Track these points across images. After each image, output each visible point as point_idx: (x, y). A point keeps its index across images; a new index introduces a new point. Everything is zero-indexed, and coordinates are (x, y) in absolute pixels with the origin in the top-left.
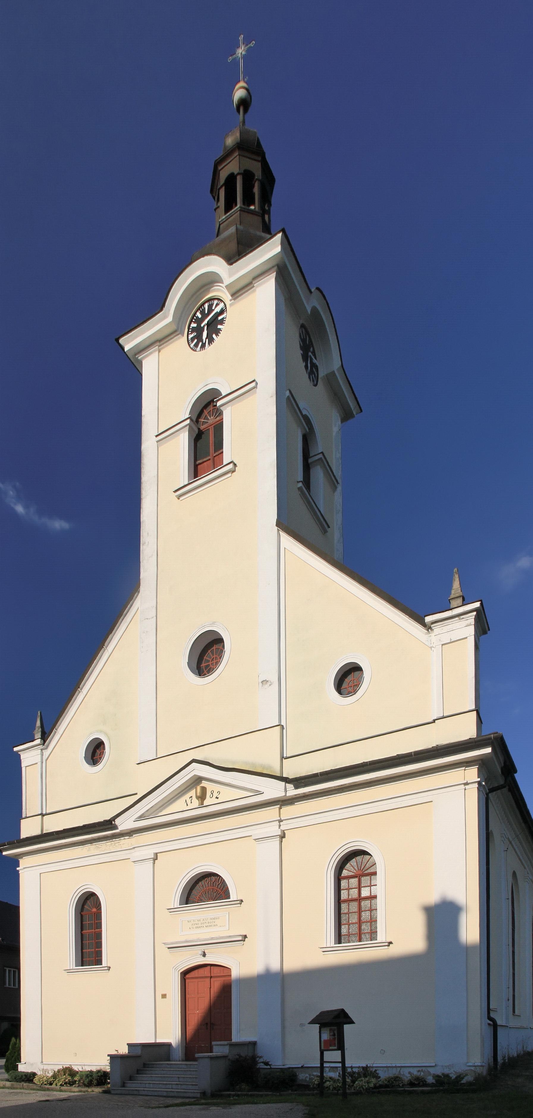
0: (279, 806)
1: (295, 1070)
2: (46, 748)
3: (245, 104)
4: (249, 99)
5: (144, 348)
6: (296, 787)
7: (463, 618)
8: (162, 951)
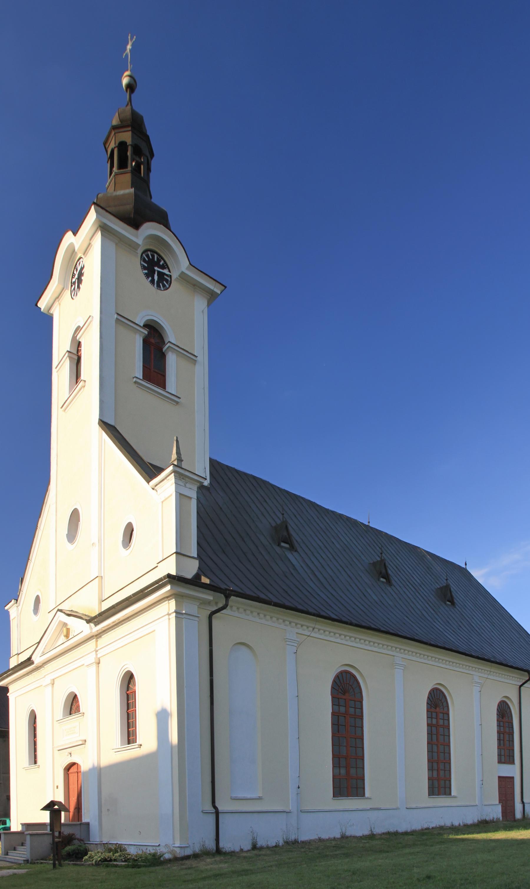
0: (94, 640)
3: (131, 87)
4: (133, 82)
6: (96, 625)
8: (56, 752)
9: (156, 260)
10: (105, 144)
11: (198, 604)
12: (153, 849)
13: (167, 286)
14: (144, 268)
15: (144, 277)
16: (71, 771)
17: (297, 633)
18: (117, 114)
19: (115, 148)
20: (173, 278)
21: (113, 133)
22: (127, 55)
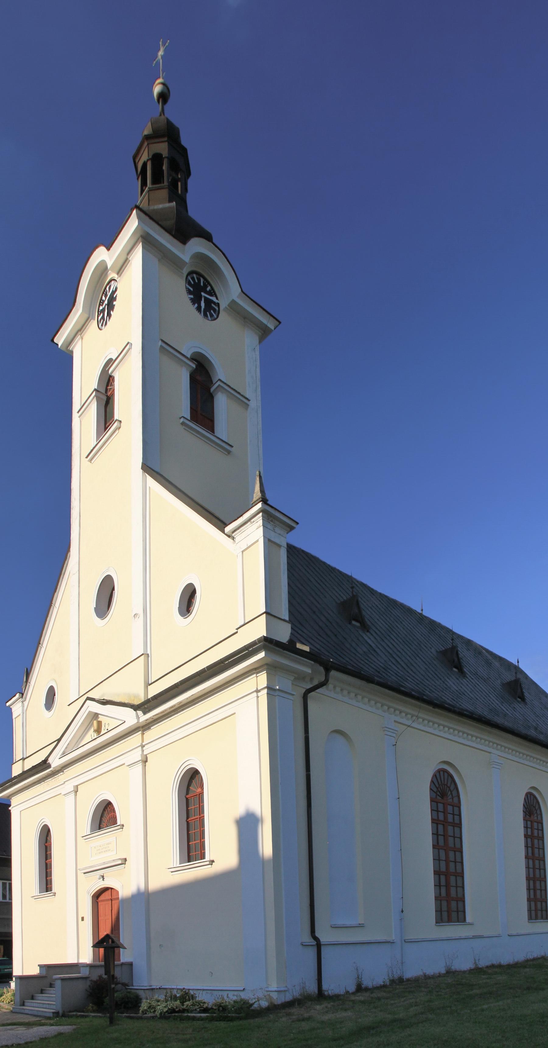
0: (140, 732)
1: (137, 991)
2: (25, 700)
3: (164, 97)
4: (166, 91)
5: (70, 341)
6: (145, 713)
7: (254, 522)
9: (202, 284)
10: (134, 158)
11: (292, 678)
12: (234, 995)
13: (215, 316)
14: (189, 292)
15: (190, 303)
16: (101, 898)
17: (395, 721)
18: (150, 124)
19: (148, 160)
20: (222, 308)
21: (146, 144)
22: (158, 63)
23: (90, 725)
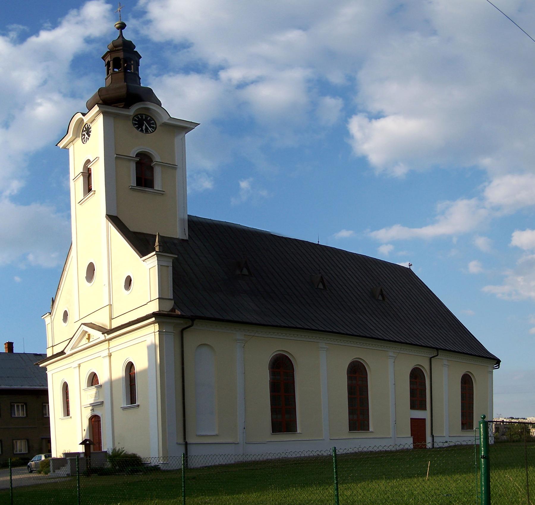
23: (84, 335)
